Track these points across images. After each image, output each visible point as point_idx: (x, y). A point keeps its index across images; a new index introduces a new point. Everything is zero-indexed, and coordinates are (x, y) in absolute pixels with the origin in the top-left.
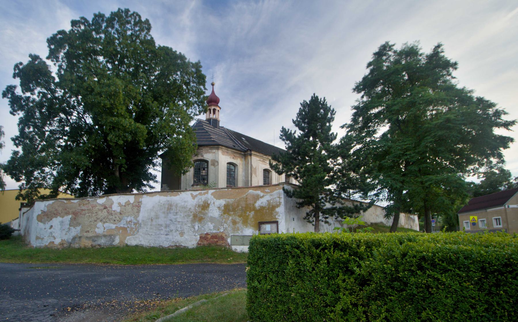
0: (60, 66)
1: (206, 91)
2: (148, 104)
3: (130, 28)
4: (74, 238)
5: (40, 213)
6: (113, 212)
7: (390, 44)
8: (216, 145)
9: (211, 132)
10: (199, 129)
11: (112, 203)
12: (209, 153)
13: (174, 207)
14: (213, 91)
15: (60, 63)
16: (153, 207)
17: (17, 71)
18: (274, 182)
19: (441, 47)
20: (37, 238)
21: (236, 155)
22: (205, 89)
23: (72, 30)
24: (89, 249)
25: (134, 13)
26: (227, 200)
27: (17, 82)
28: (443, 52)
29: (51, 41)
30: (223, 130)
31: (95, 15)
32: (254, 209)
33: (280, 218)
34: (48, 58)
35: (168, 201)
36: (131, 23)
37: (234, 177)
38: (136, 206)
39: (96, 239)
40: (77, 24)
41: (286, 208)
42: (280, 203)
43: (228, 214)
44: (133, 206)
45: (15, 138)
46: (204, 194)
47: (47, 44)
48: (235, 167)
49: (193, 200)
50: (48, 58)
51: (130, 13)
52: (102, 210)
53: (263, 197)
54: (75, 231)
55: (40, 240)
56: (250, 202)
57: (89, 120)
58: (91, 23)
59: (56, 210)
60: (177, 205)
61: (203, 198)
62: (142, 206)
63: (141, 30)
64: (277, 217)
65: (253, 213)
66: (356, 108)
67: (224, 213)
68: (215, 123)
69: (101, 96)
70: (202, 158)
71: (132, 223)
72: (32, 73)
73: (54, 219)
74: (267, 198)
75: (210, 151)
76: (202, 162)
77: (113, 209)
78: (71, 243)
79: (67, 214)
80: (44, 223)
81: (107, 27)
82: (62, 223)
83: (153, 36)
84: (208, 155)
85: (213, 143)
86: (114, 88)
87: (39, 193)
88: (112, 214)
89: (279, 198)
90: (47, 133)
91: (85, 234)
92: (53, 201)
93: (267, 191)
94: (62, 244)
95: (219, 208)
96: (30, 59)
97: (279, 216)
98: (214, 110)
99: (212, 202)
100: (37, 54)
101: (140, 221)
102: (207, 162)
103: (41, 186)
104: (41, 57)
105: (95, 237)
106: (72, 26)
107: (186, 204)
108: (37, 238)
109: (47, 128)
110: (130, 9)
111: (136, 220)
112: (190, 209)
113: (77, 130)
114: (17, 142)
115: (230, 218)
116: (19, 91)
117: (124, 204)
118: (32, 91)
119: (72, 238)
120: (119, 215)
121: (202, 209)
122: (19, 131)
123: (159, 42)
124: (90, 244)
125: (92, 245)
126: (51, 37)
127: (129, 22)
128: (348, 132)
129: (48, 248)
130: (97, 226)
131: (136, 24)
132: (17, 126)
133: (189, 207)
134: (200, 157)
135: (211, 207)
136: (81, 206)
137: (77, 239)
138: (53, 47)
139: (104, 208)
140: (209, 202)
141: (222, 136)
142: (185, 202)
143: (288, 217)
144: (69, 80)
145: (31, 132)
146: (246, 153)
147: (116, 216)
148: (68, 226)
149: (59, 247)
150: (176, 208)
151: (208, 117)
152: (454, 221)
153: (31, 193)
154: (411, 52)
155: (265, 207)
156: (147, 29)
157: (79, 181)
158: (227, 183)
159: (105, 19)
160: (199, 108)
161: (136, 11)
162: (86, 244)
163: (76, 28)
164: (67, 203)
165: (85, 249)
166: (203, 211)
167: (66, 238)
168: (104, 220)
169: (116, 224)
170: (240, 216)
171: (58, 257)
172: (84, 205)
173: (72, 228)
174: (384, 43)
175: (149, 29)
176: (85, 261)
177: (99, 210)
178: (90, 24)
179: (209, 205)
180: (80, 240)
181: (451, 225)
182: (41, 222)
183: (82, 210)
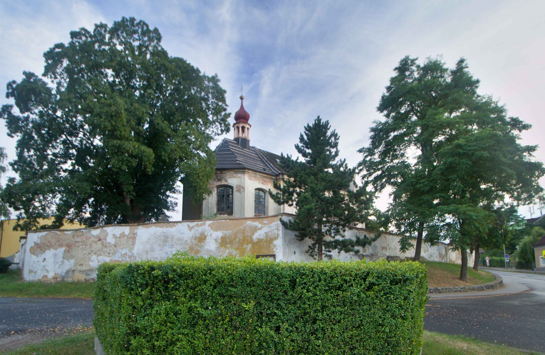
0: (59, 84)
1: (227, 107)
2: (158, 124)
3: (138, 38)
4: (68, 272)
5: (33, 245)
6: (107, 244)
7: (411, 57)
8: (241, 169)
9: (238, 154)
10: (224, 150)
11: (107, 235)
12: (234, 177)
13: (170, 240)
14: (242, 106)
15: (58, 80)
16: (149, 239)
17: (10, 91)
18: (271, 212)
19: (465, 62)
20: (31, 271)
21: (265, 180)
22: (226, 105)
23: (72, 42)
24: (82, 283)
25: (141, 21)
26: (225, 232)
27: (12, 101)
28: (467, 67)
29: (49, 55)
30: (254, 151)
31: (97, 26)
32: (251, 242)
33: (278, 251)
34: (44, 75)
35: (164, 233)
36: (138, 33)
37: (264, 205)
38: (131, 238)
39: (89, 273)
40: (77, 35)
41: (285, 240)
42: (278, 235)
43: (225, 247)
44: (128, 237)
45: (13, 162)
46: (201, 225)
47: (44, 59)
48: (265, 193)
49: (189, 232)
50: (44, 75)
51: (135, 22)
52: (96, 242)
53: (261, 228)
54: (69, 265)
55: (33, 274)
56: (248, 234)
57: (97, 141)
58: (92, 34)
59: (49, 242)
60: (173, 237)
61: (200, 229)
62: (137, 238)
63: (151, 40)
64: (274, 250)
65: (250, 245)
66: (373, 130)
67: (221, 246)
68: (243, 142)
69: (101, 117)
70: (226, 183)
71: (127, 256)
72: (27, 91)
73: (47, 252)
74: (266, 229)
75: (235, 175)
76: (226, 188)
77: (108, 242)
78: (64, 277)
79: (61, 246)
80: (38, 256)
81: (111, 38)
82: (55, 255)
83: (163, 47)
84: (232, 180)
85: (236, 166)
86: (115, 108)
87: (38, 223)
88: (106, 247)
89: (278, 229)
90: (50, 157)
91: (79, 268)
92: (46, 233)
93: (265, 222)
94: (55, 278)
95: (216, 240)
96: (24, 77)
97: (277, 249)
98: (243, 128)
99: (209, 234)
100: (32, 71)
101: (135, 254)
102: (232, 188)
103: (40, 215)
104: (36, 74)
105: (89, 270)
106: (72, 38)
107: (182, 235)
108: (31, 271)
109: (49, 152)
110: (136, 18)
111: (131, 252)
112: (186, 241)
113: (83, 153)
114: (16, 167)
115: (227, 251)
116: (16, 111)
117: (119, 236)
118: (29, 110)
119: (65, 271)
120: (113, 247)
121: (199, 241)
122: (17, 155)
123: (172, 53)
124: (84, 278)
125: (85, 279)
126: (48, 52)
127: (135, 32)
128: (366, 157)
129: (41, 282)
130: (92, 259)
131: (144, 34)
132: (15, 149)
133: (185, 239)
134: (223, 183)
135: (208, 240)
136: (75, 238)
137: (70, 273)
138: (50, 62)
139: (99, 240)
140: (206, 234)
141: (251, 158)
142: (181, 233)
143: (287, 250)
144: (66, 100)
145: (32, 156)
146: (278, 178)
147: (111, 248)
148: (62, 259)
149: (52, 281)
150: (172, 240)
151: (236, 136)
152: (530, 256)
153: (30, 223)
154: (433, 68)
155: (263, 240)
156: (157, 39)
157: (89, 210)
158: (255, 212)
159: (108, 29)
160: (221, 126)
161: (143, 19)
162: (80, 278)
163: (76, 40)
164: (60, 235)
165: (79, 283)
166: (199, 244)
167: (59, 271)
168: (98, 253)
169: (110, 257)
170: (237, 249)
171: (48, 292)
172: (78, 236)
173: (65, 261)
174: (404, 57)
175: (159, 39)
176: (75, 295)
177: (93, 242)
178: (91, 35)
179: (205, 237)
180: (73, 274)
181: (527, 260)
182: (34, 254)
183: (76, 242)
